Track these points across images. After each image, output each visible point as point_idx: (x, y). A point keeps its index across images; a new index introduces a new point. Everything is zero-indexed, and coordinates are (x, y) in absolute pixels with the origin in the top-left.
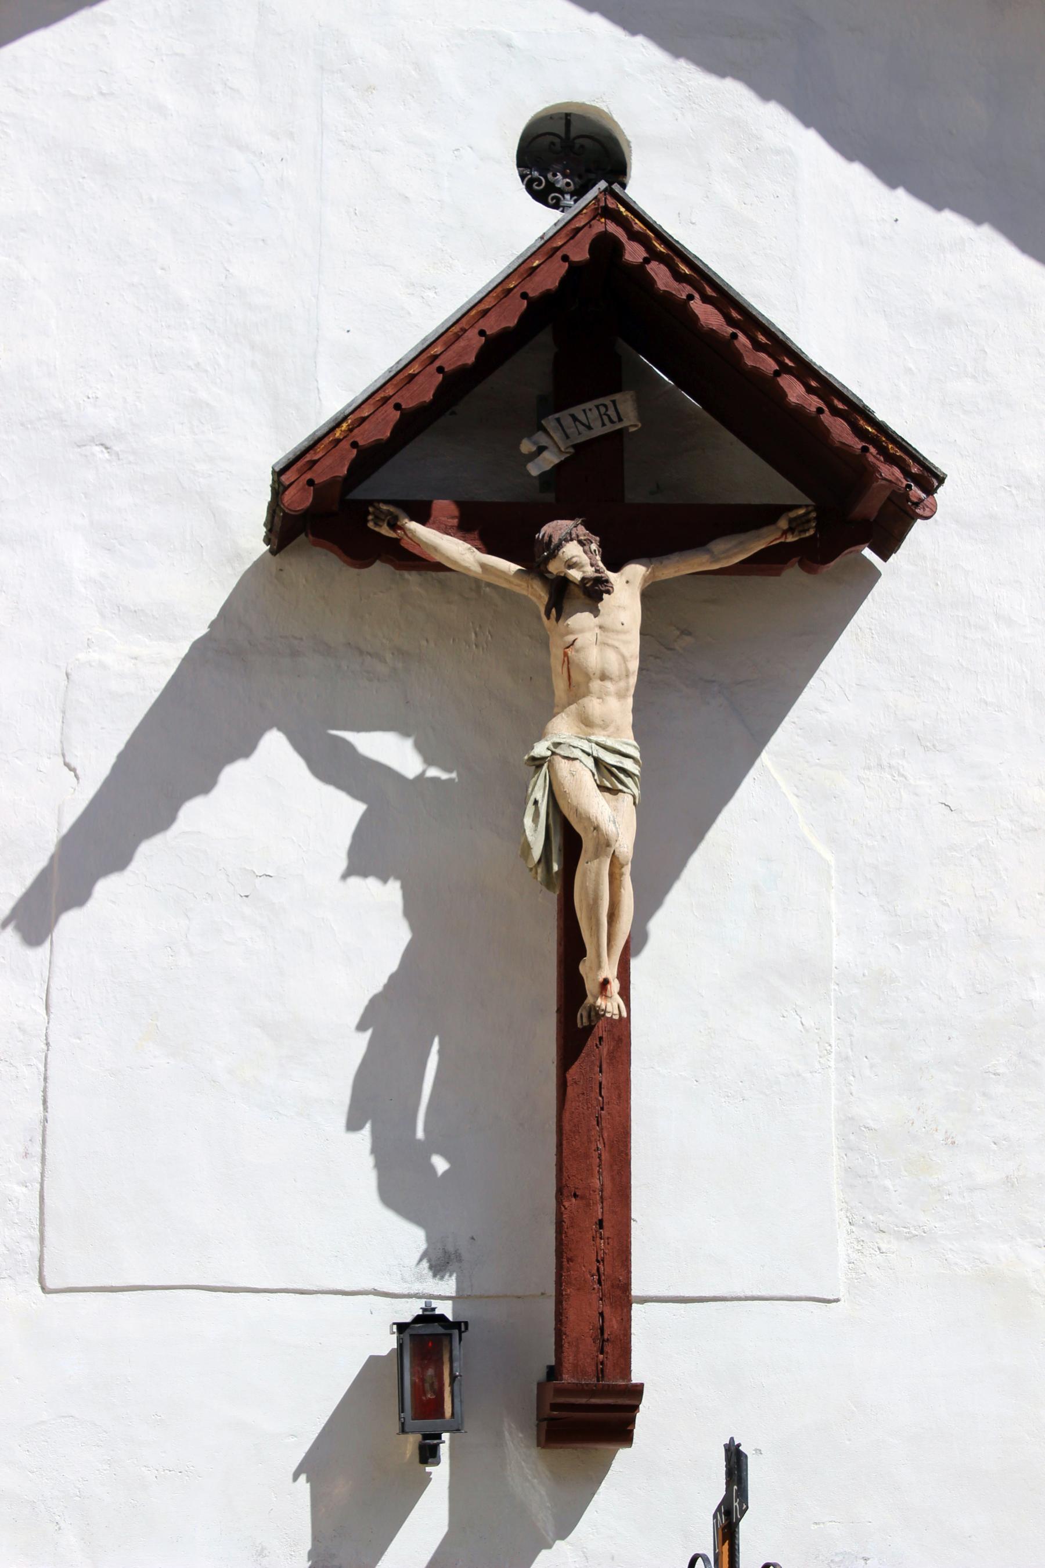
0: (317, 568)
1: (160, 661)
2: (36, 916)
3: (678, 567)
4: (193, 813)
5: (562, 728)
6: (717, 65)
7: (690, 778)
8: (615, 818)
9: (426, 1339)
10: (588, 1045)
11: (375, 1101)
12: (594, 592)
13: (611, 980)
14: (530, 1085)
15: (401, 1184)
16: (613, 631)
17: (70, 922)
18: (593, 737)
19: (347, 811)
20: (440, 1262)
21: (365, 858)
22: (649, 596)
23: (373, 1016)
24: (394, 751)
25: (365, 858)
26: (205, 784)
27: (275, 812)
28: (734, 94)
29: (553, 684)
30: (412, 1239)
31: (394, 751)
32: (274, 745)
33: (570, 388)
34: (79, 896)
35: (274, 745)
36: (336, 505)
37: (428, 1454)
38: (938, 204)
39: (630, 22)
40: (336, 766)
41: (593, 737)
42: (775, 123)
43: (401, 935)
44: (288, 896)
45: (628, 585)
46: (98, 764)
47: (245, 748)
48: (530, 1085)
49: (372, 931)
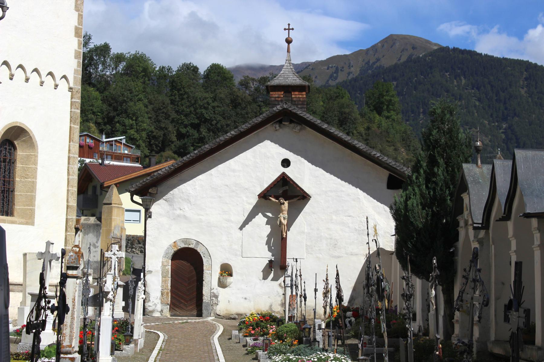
0: (263, 200)
1: (251, 207)
2: (241, 228)
3: (290, 201)
4: (253, 220)
5: (281, 214)
6: (298, 155)
7: (292, 220)
8: (285, 222)
9: (271, 261)
10: (284, 240)
11: (268, 243)
12: (284, 203)
13: (220, 289)
14: (278, 243)
15: (270, 250)
16: (286, 205)
17: (244, 229)
18: (283, 217)
19: (266, 219)
20: (273, 256)
21: (267, 223)
22: (288, 203)
23: (268, 236)
24: (269, 214)
25: (267, 223)
26: (254, 218)
27: (260, 219)
28: (299, 157)
29: (281, 211)
30: (271, 254)
31: (269, 214)
32: (260, 214)
33: (283, 186)
34: (245, 227)
35: (260, 214)
36: (264, 196)
37: (272, 270)
38: (317, 166)
39: (291, 151)
40: (265, 216)
41: (283, 217)
42: (303, 160)
43: (270, 230)
44: (261, 226)
45: (286, 203)
46: (246, 216)
47: (258, 215)
48: (278, 243)
49: (268, 229)
